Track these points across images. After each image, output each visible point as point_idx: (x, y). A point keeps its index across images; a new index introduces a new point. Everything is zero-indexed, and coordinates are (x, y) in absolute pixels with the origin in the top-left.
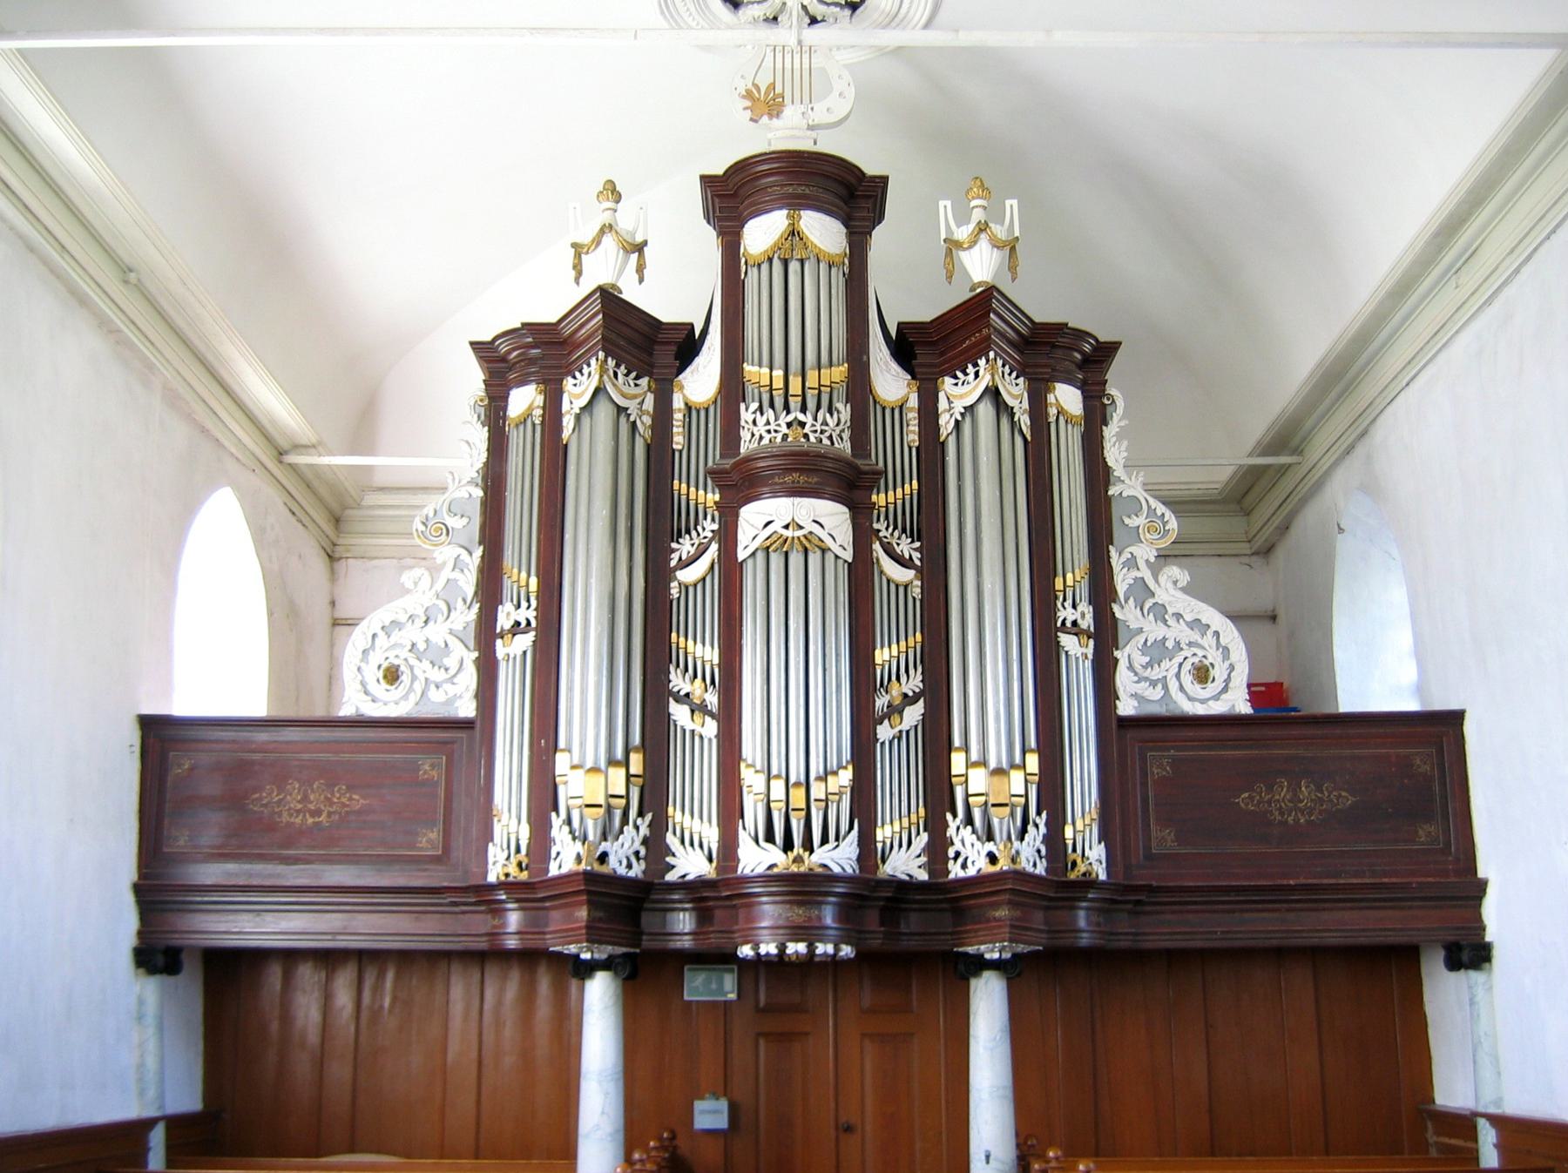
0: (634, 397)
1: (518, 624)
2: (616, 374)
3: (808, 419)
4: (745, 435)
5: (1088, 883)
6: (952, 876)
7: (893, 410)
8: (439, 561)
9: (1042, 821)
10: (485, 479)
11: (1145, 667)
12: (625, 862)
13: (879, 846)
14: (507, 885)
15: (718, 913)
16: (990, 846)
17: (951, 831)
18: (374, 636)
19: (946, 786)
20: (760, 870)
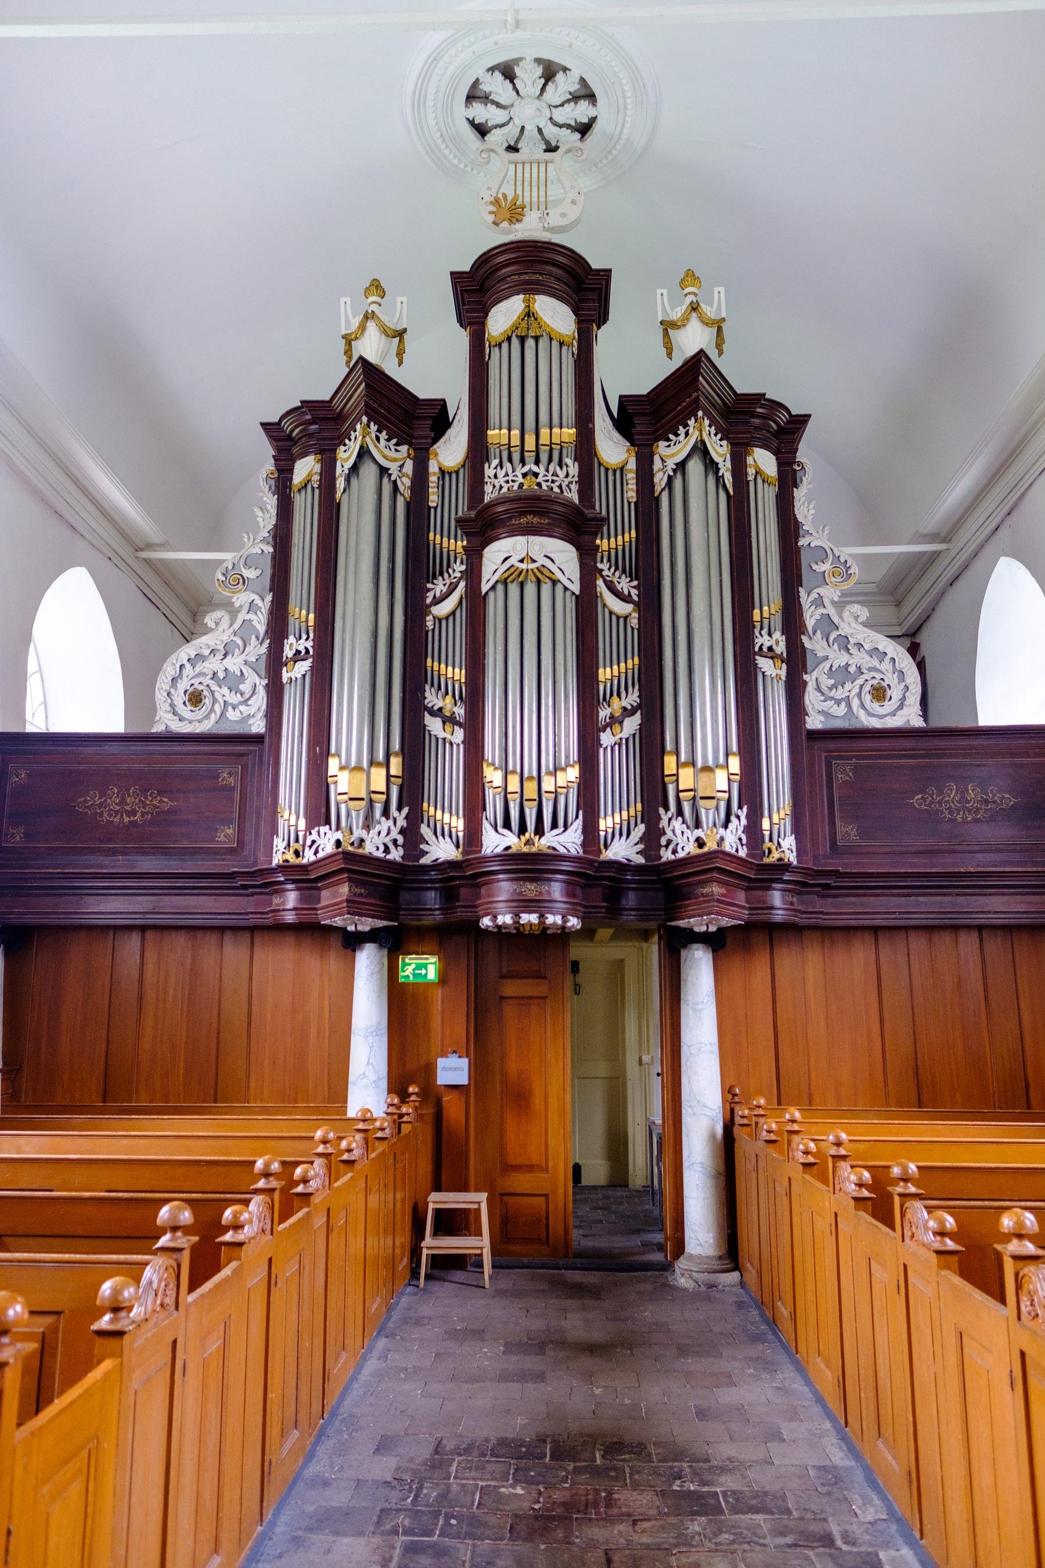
0: (395, 460)
1: (298, 652)
2: (378, 439)
3: (541, 470)
4: (488, 489)
5: (782, 866)
6: (664, 859)
7: (615, 471)
8: (237, 605)
9: (743, 813)
10: (275, 538)
11: (831, 689)
12: (382, 848)
13: (602, 834)
14: (285, 868)
15: (463, 891)
16: (699, 833)
17: (664, 823)
18: (182, 666)
19: (660, 787)
20: (499, 850)
